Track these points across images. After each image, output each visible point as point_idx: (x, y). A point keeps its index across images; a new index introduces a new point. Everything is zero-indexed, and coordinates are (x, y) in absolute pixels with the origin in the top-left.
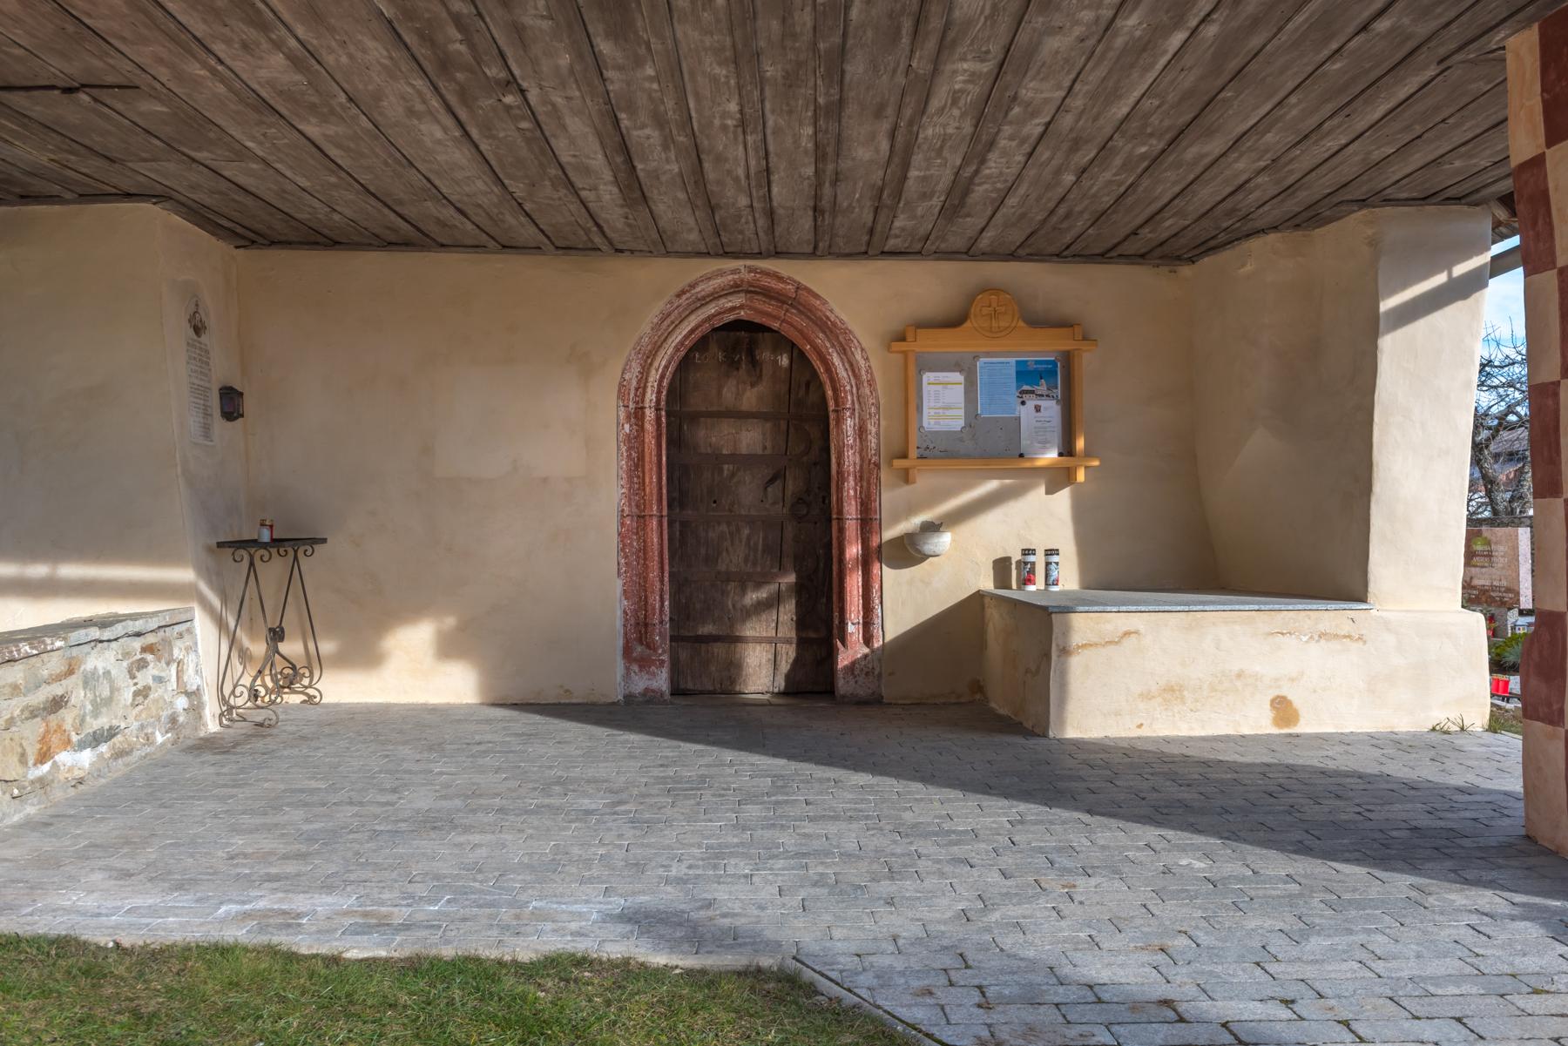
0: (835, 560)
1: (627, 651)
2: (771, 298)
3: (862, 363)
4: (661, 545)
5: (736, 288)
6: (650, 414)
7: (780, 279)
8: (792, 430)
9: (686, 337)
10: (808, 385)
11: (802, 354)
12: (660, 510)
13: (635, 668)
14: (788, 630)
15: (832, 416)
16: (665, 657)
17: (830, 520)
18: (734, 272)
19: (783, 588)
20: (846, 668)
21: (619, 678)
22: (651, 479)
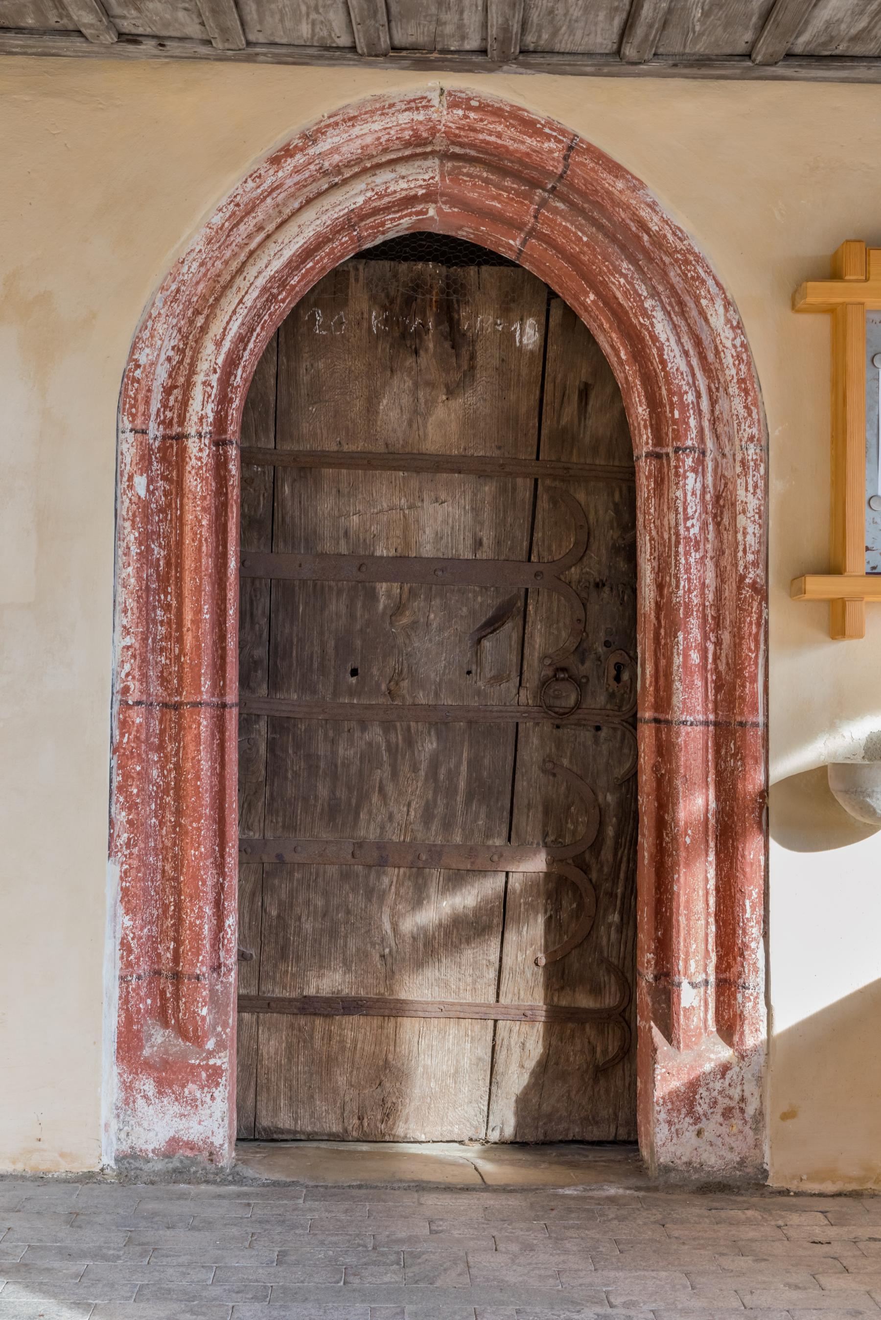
0: (647, 822)
1: (129, 1044)
2: (504, 172)
3: (726, 336)
4: (221, 777)
5: (417, 147)
6: (198, 452)
7: (529, 125)
8: (544, 503)
9: (293, 265)
10: (584, 393)
11: (571, 316)
12: (219, 689)
13: (148, 1086)
14: (527, 989)
15: (645, 468)
16: (224, 1060)
17: (633, 722)
18: (415, 104)
19: (516, 882)
20: (673, 1097)
21: (106, 1112)
22: (197, 613)
